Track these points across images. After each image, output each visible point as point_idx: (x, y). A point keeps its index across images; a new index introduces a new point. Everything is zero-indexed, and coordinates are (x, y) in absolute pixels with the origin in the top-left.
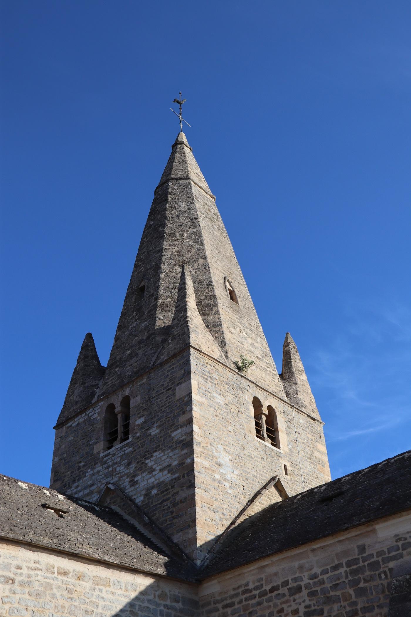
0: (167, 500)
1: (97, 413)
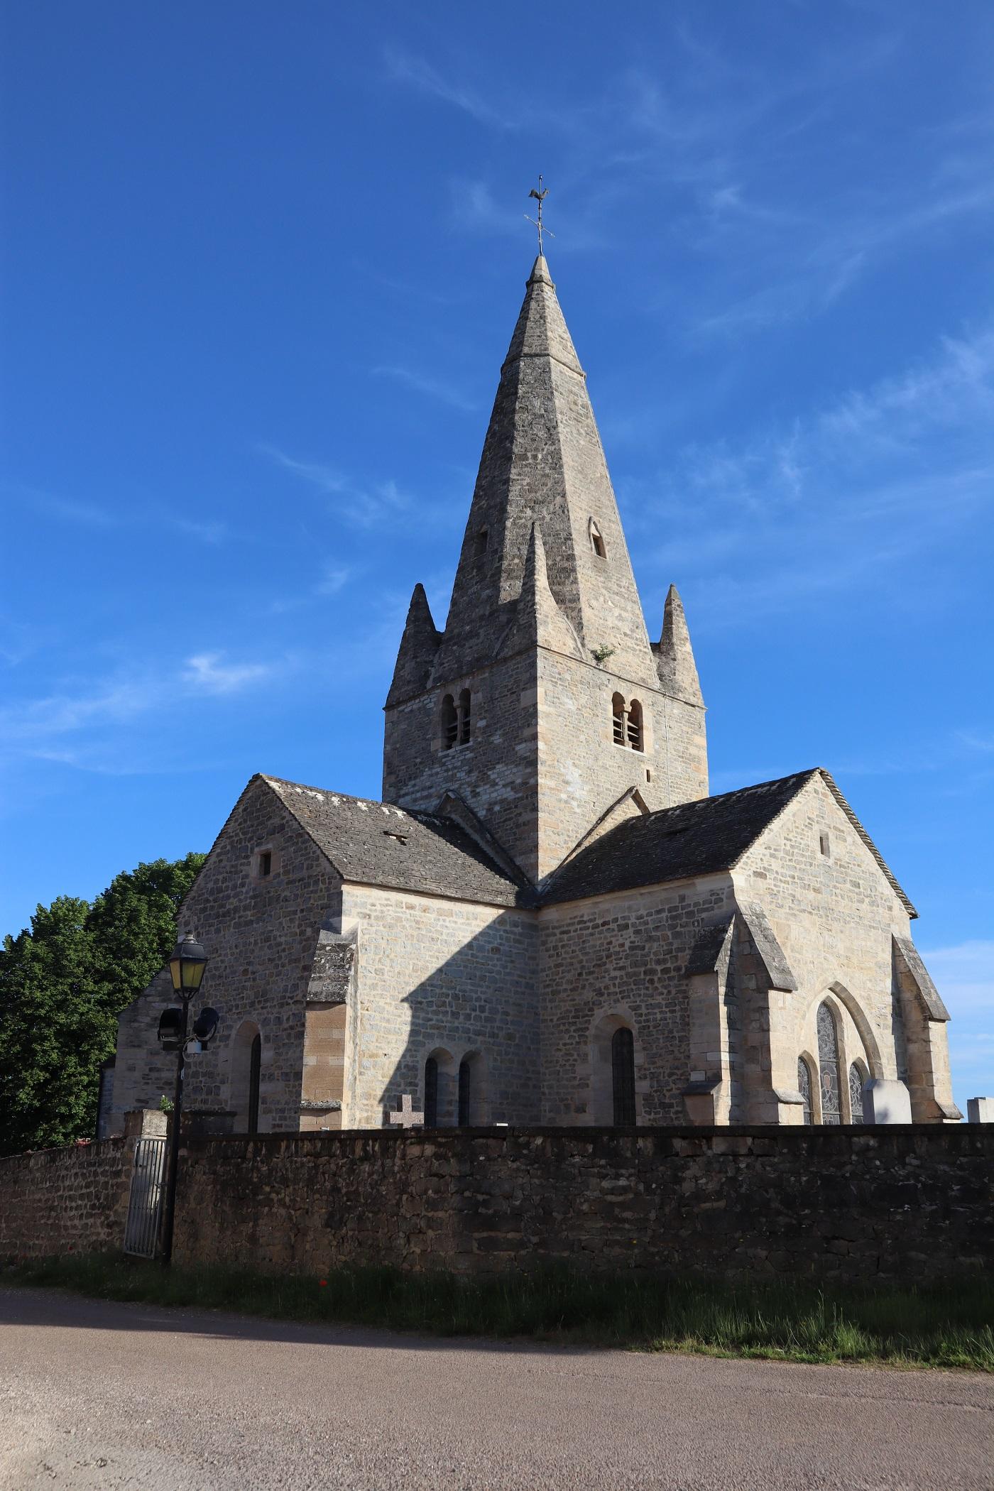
0: (510, 819)
1: (433, 702)
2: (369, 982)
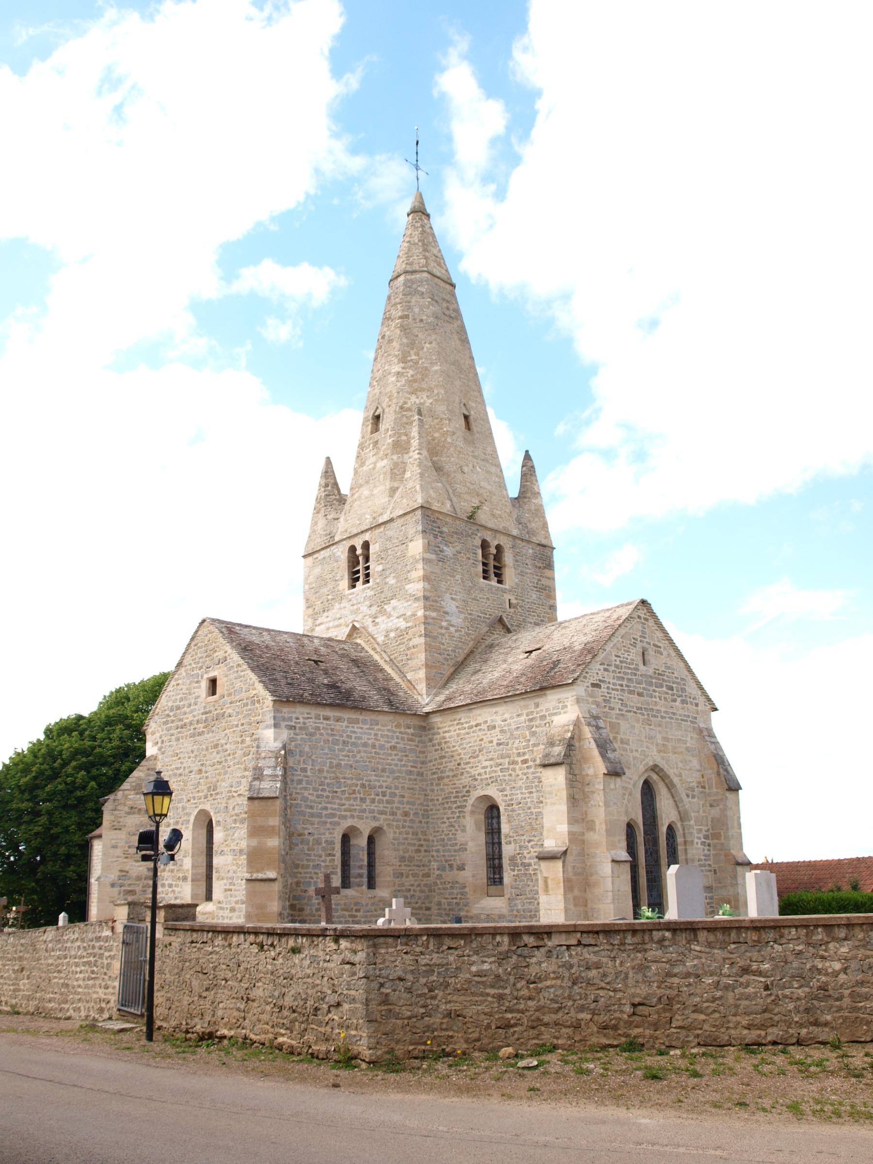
2: (296, 778)
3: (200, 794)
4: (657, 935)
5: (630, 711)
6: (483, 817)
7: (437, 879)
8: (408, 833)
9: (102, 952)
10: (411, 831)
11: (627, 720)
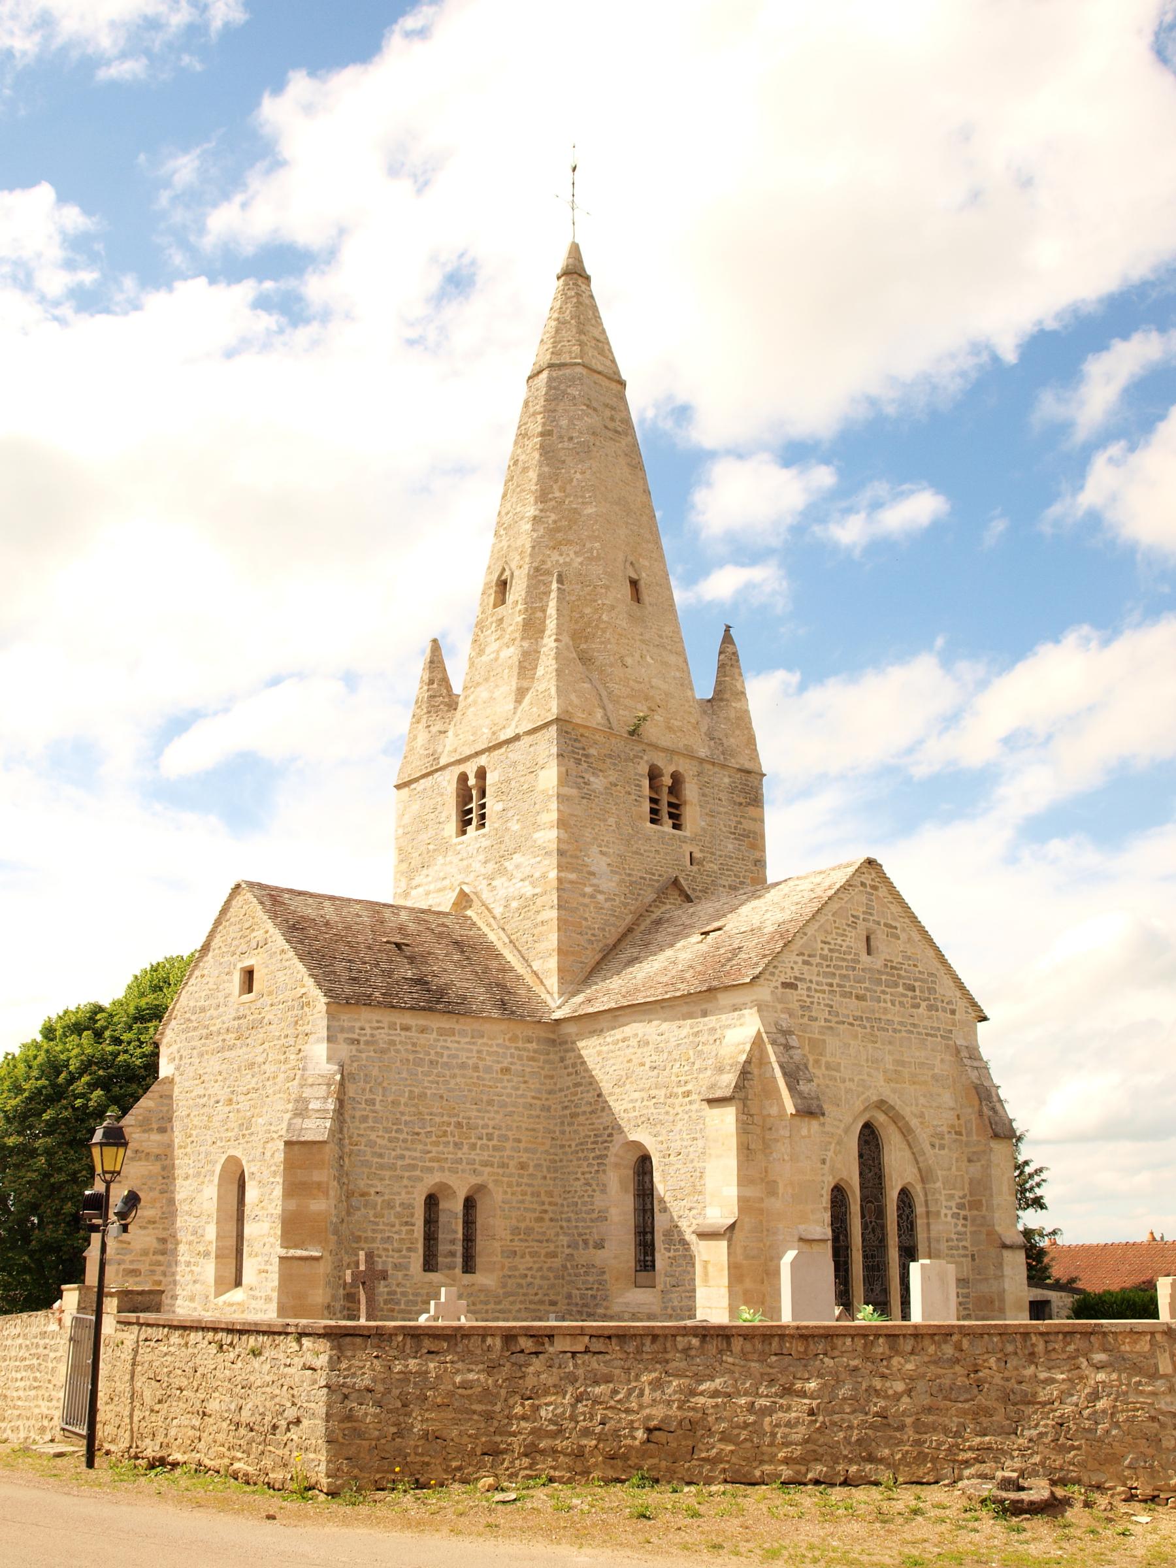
2: (358, 1114)
3: (229, 1134)
4: (681, 1342)
5: (844, 1023)
6: (631, 1172)
7: (567, 1260)
8: (524, 1194)
9: (46, 1352)
10: (529, 1190)
11: (838, 1035)
